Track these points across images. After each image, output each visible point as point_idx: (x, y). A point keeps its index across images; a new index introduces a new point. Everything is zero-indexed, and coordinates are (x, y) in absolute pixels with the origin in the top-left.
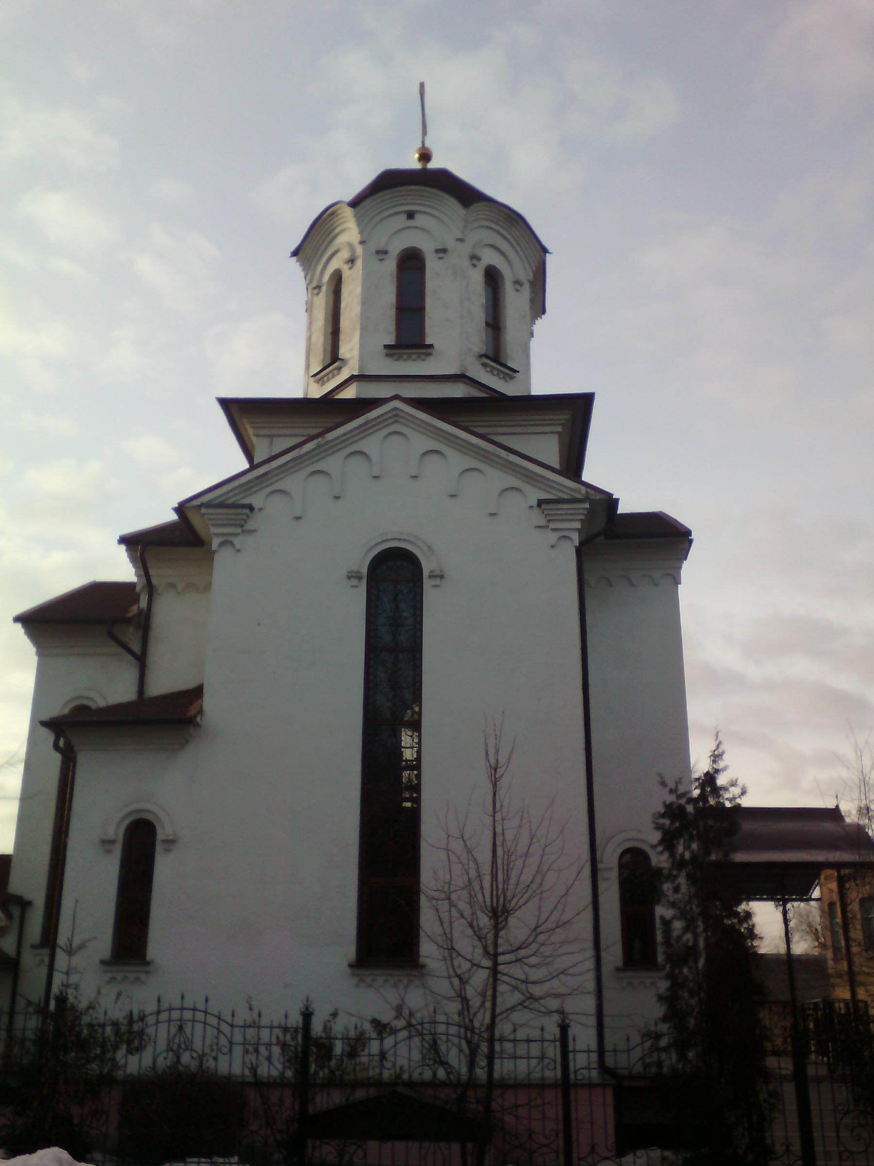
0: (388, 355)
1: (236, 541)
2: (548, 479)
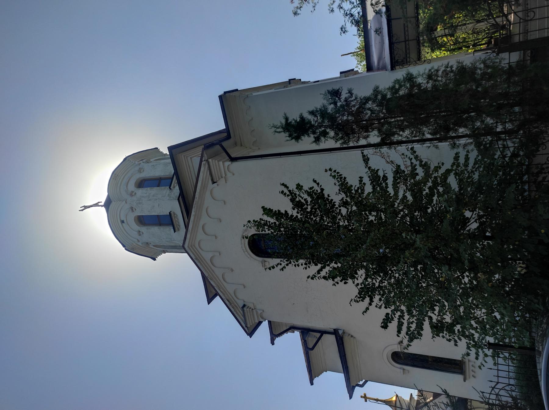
0: (179, 230)
1: (259, 312)
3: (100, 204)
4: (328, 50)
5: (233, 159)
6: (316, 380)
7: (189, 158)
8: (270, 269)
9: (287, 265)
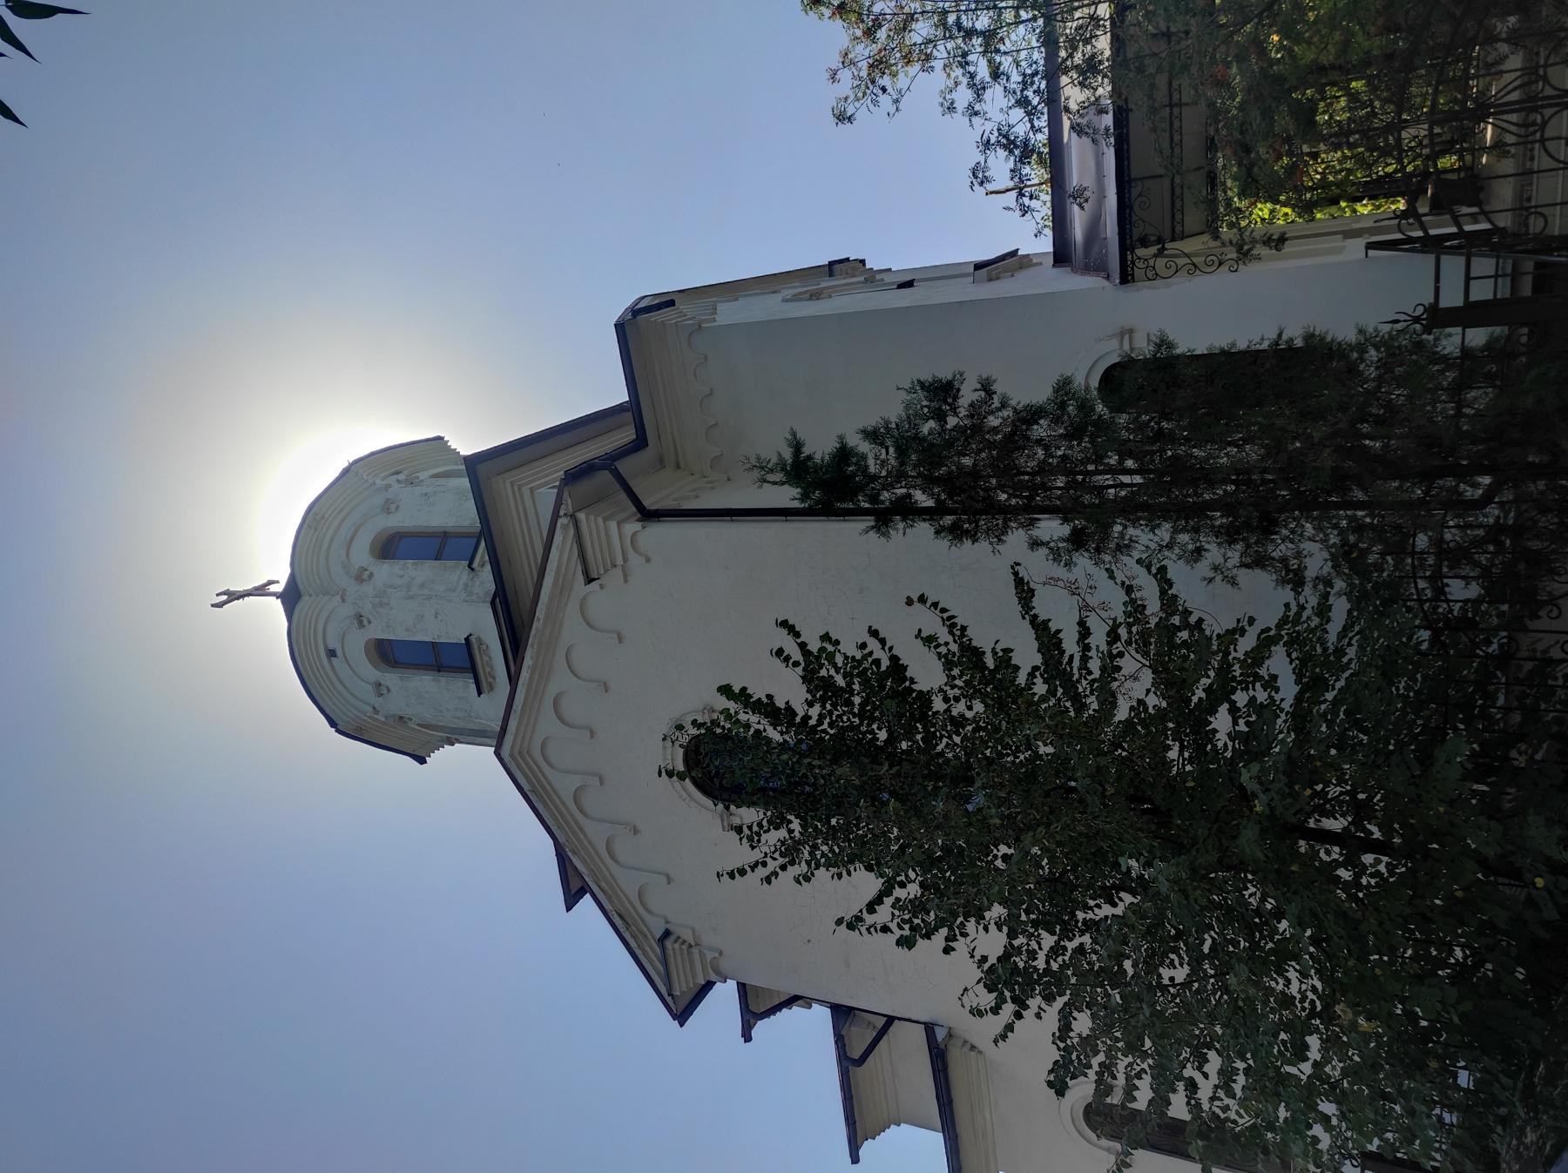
0: (491, 688)
1: (709, 955)
2: (559, 567)
3: (273, 588)
4: (938, 190)
5: (649, 515)
6: (867, 1148)
7: (526, 491)
8: (732, 875)
9: (783, 868)
